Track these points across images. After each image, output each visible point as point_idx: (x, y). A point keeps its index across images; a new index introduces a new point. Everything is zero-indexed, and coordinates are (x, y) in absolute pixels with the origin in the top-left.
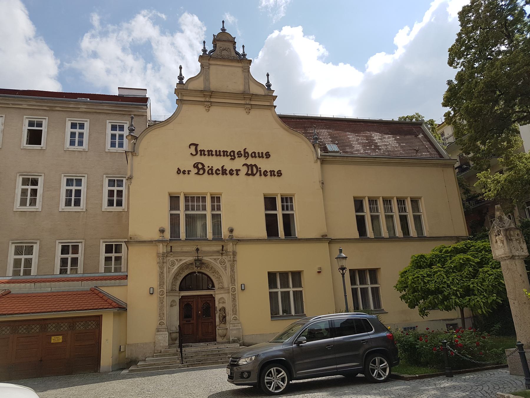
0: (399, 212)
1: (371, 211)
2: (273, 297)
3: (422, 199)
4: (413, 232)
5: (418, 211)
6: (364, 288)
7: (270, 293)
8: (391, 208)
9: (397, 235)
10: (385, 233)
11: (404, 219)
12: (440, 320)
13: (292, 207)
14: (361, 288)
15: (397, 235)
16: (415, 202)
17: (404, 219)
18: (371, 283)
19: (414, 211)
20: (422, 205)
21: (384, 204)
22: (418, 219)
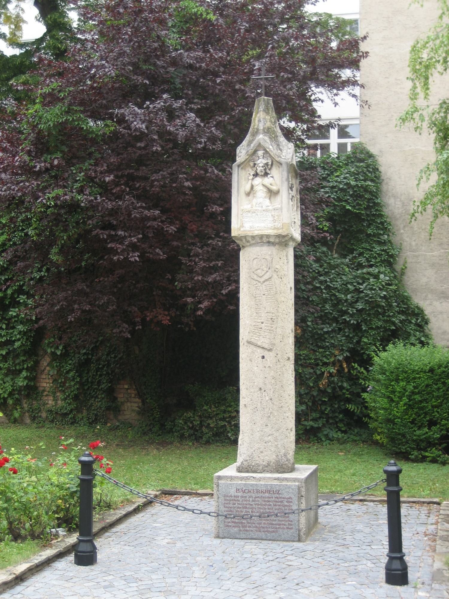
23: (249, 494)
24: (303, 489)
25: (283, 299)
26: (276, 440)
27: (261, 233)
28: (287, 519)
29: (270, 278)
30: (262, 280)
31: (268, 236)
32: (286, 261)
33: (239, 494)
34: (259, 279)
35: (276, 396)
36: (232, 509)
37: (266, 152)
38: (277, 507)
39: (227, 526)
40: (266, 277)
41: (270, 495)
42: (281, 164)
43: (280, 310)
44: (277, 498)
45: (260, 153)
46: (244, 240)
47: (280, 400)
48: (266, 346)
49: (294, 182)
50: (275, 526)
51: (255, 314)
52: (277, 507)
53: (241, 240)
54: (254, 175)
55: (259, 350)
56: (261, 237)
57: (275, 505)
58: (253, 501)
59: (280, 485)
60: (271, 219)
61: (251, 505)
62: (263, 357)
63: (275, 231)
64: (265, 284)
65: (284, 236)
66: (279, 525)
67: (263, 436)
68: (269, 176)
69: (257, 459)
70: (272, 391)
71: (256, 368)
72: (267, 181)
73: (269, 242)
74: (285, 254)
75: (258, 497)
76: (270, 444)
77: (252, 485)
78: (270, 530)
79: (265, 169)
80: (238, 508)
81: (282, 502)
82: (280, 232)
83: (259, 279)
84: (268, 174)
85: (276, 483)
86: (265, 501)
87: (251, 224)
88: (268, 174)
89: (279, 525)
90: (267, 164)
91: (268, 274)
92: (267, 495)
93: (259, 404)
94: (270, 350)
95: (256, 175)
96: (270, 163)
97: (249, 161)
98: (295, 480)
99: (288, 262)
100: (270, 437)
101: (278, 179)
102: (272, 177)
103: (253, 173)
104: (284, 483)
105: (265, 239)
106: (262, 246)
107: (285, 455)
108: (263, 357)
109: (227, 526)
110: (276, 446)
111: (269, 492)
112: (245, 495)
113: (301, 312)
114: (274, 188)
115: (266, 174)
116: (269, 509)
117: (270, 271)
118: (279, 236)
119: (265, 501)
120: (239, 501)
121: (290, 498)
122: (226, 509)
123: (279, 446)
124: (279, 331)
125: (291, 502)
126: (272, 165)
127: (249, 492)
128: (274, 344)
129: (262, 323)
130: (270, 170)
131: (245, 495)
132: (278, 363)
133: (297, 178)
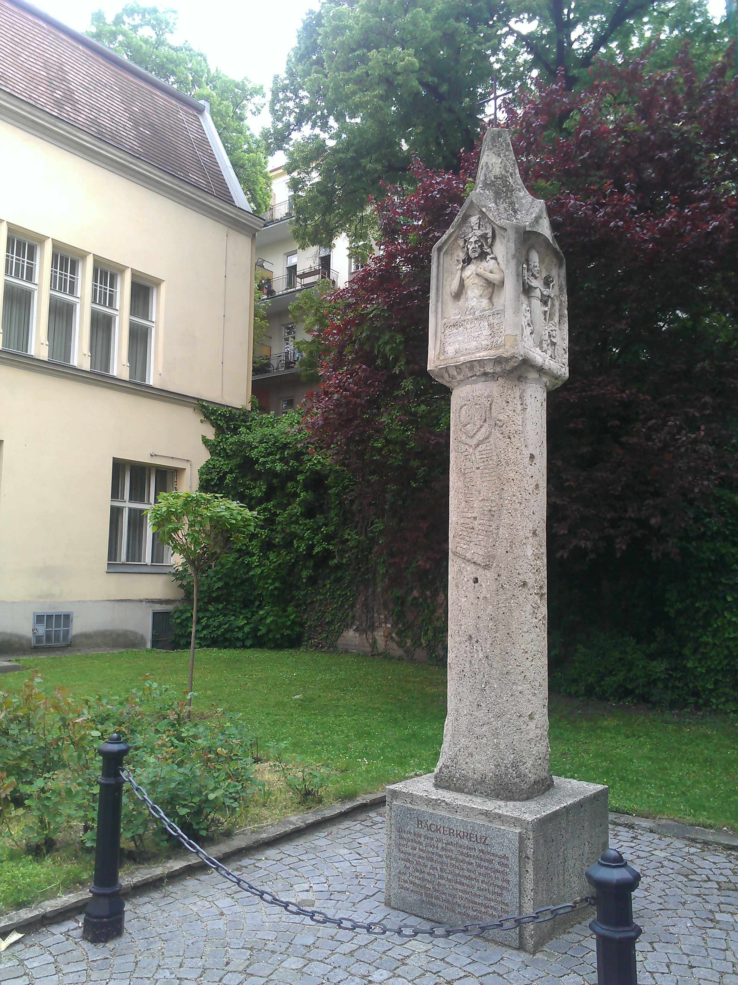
0: (94, 302)
1: (53, 287)
2: (116, 513)
3: (163, 287)
4: (120, 366)
5: (146, 315)
6: (135, 510)
7: (112, 508)
8: (111, 296)
9: (33, 351)
10: (80, 355)
11: (102, 325)
12: (141, 601)
13: (73, 285)
14: (130, 509)
15: (33, 351)
16: (143, 291)
17: (102, 325)
18: (132, 498)
19: (133, 311)
20: (161, 305)
21: (95, 279)
22: (139, 337)
23: (438, 835)
24: (530, 844)
25: (512, 475)
26: (496, 735)
27: (468, 358)
28: (499, 899)
29: (487, 438)
30: (474, 442)
31: (481, 362)
32: (519, 407)
33: (423, 832)
34: (469, 441)
35: (497, 651)
36: (411, 858)
37: (483, 216)
38: (483, 870)
39: (402, 888)
40: (480, 436)
41: (470, 845)
42: (505, 230)
43: (506, 495)
44: (481, 851)
45: (474, 220)
46: (446, 376)
47: (504, 660)
48: (479, 560)
49: (554, 273)
50: (476, 907)
51: (463, 504)
52: (483, 870)
53: (442, 377)
54: (464, 261)
55: (470, 568)
56: (471, 364)
57: (479, 866)
58: (443, 849)
59: (488, 828)
60: (487, 332)
61: (441, 856)
62: (476, 581)
63: (493, 352)
64: (479, 449)
65: (507, 360)
66: (486, 907)
67: (472, 724)
68: (488, 257)
69: (464, 767)
70: (489, 642)
71: (463, 600)
72: (486, 266)
73: (485, 374)
74: (517, 395)
75: (451, 844)
76: (484, 741)
77: (442, 818)
78: (471, 913)
79: (481, 247)
80: (420, 857)
81: (490, 861)
82: (499, 352)
83: (469, 441)
84: (488, 254)
85: (481, 821)
86: (462, 854)
87: (457, 346)
88: (488, 254)
89: (486, 907)
90: (484, 237)
91: (483, 430)
92: (466, 842)
93: (468, 665)
94: (487, 567)
95: (468, 261)
96: (490, 235)
97: (456, 239)
98: (517, 822)
99: (524, 410)
100: (485, 728)
101: (502, 259)
102: (495, 259)
103: (462, 256)
104: (496, 825)
105: (478, 370)
106: (475, 382)
107: (515, 766)
108: (476, 581)
109: (402, 888)
110: (497, 745)
111: (469, 836)
112: (431, 834)
113: (553, 499)
114: (495, 277)
115: (483, 256)
116: (468, 870)
117: (486, 425)
118: (498, 361)
119: (462, 854)
120: (421, 844)
121: (505, 857)
122: (402, 855)
123: (502, 747)
124: (503, 532)
125: (506, 866)
126: (494, 237)
127: (437, 830)
128: (494, 557)
129: (475, 518)
130: (491, 246)
131: (431, 834)
132: (501, 592)
133: (560, 266)
